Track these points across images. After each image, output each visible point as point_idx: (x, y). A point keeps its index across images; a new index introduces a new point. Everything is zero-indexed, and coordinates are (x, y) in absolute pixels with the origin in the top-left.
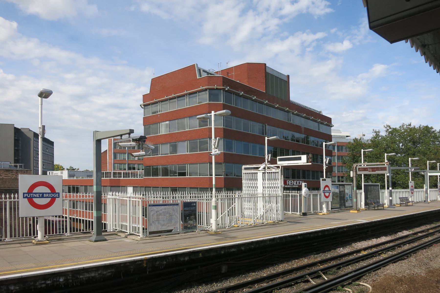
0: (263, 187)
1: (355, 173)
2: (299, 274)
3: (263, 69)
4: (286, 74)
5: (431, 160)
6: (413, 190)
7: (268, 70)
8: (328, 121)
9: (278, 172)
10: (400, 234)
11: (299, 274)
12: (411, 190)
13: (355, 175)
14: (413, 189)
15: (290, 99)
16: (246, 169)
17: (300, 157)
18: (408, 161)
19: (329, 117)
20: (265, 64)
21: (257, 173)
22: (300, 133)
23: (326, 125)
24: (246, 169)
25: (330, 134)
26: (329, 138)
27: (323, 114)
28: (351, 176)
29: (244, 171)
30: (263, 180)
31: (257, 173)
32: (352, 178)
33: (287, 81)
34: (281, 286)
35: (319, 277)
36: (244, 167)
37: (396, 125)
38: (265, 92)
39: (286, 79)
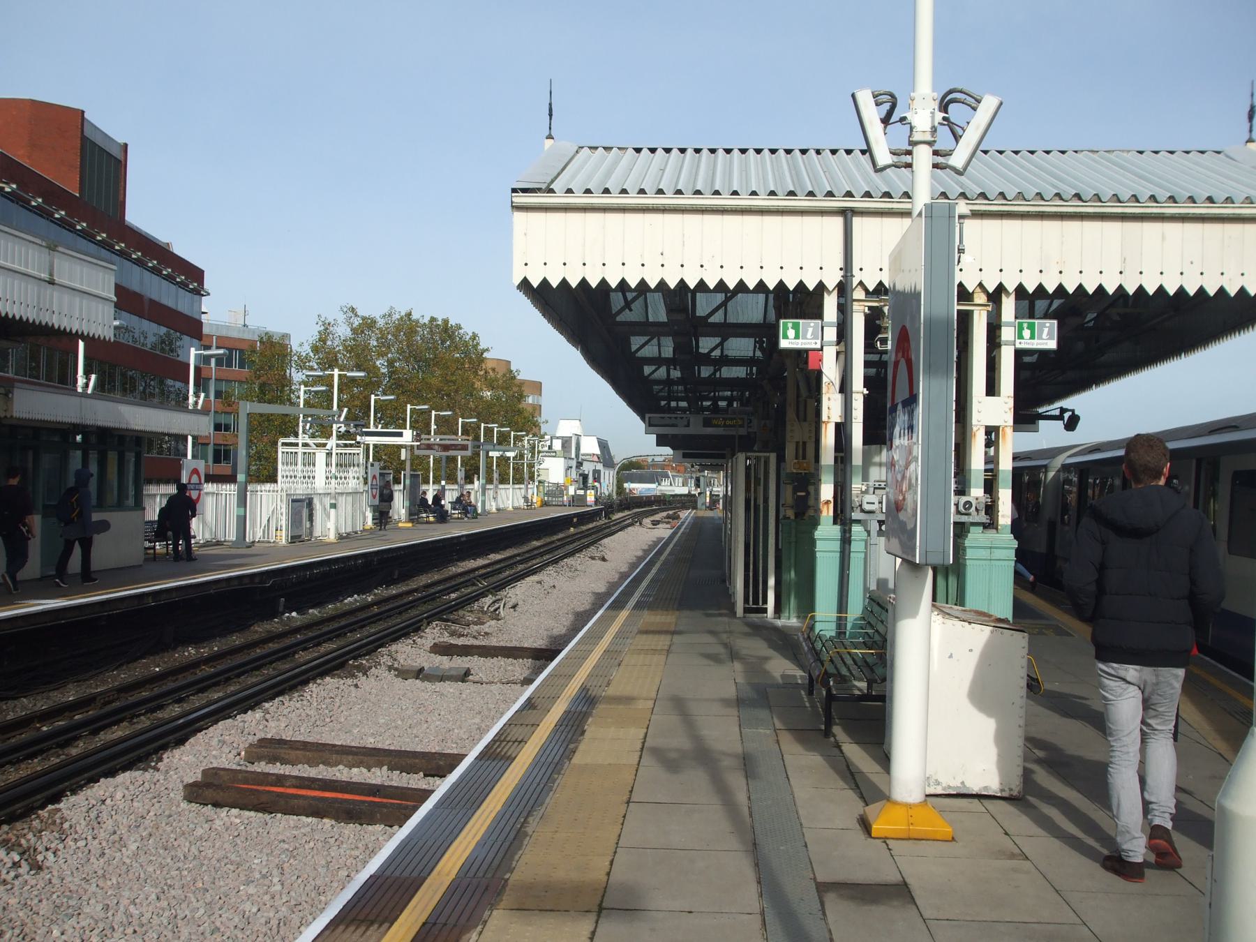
0: (327, 478)
1: (409, 452)
2: (467, 578)
3: (77, 127)
4: (121, 140)
5: (502, 426)
6: (200, 490)
7: (87, 133)
8: (191, 277)
9: (358, 454)
10: (454, 570)
11: (467, 578)
12: (372, 489)
13: (409, 457)
14: (200, 483)
15: (126, 218)
16: (284, 444)
17: (402, 433)
18: (458, 424)
19: (184, 260)
20: (83, 112)
21: (314, 453)
22: (140, 317)
23: (192, 291)
24: (284, 444)
25: (186, 311)
26: (193, 328)
27: (175, 252)
28: (403, 457)
29: (280, 449)
30: (327, 465)
31: (314, 453)
32: (405, 461)
33: (121, 161)
34: (449, 591)
35: (474, 584)
36: (282, 440)
37: (375, 307)
38: (78, 195)
39: (116, 153)
